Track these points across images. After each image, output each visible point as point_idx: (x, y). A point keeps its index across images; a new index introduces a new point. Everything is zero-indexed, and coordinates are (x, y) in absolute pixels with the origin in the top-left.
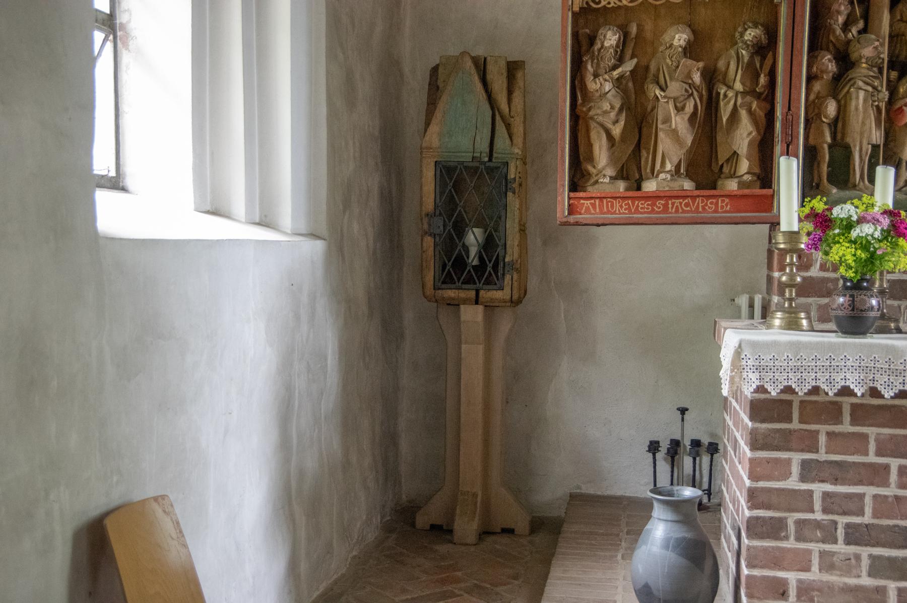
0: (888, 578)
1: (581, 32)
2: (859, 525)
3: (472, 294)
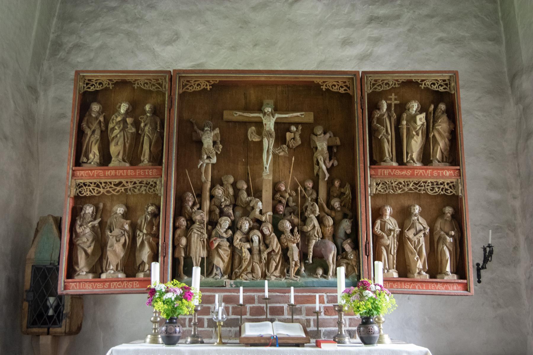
3: (46, 330)
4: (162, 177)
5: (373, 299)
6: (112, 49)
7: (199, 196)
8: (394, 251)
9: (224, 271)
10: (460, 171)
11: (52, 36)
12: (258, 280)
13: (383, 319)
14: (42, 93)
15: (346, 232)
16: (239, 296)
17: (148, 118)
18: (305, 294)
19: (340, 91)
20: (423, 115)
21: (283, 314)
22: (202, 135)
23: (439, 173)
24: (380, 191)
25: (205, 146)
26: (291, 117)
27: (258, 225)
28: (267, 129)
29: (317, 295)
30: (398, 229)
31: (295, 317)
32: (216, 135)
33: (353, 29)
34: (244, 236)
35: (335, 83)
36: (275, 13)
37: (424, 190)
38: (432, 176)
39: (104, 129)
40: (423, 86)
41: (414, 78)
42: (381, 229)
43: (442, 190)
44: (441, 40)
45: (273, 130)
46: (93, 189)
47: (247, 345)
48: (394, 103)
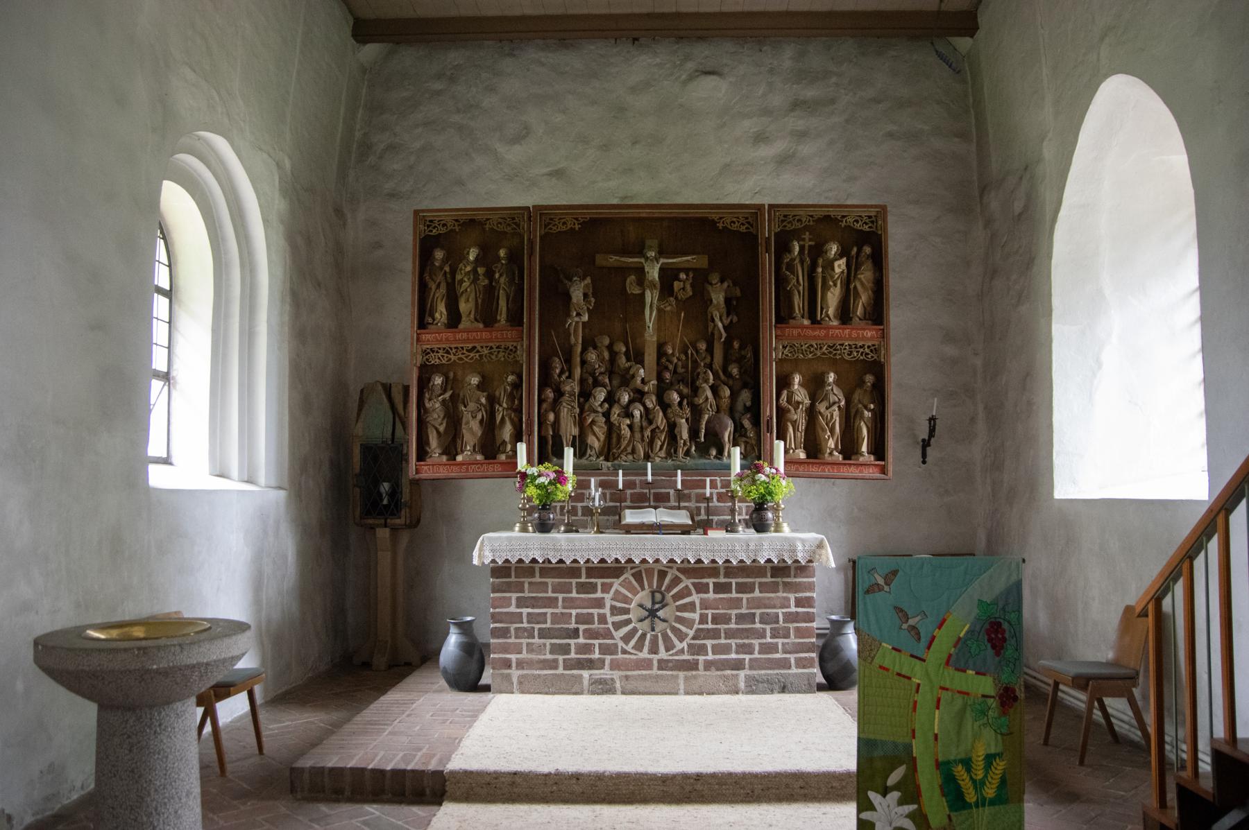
0: (559, 654)
1: (424, 376)
2: (545, 628)
3: (383, 521)
4: (523, 340)
5: (766, 484)
6: (438, 150)
7: (568, 360)
8: (802, 427)
9: (599, 451)
10: (884, 332)
11: (358, 135)
12: (640, 462)
13: (783, 506)
14: (349, 216)
15: (745, 405)
16: (618, 481)
17: (504, 267)
18: (695, 478)
19: (741, 230)
20: (844, 260)
21: (669, 501)
22: (570, 286)
23: (858, 334)
24: (787, 355)
25: (574, 300)
26: (680, 263)
27: (639, 396)
28: (650, 279)
29: (708, 480)
30: (807, 401)
31: (682, 504)
32: (587, 286)
33: (770, 119)
34: (623, 410)
35: (735, 219)
36: (662, 96)
37: (840, 355)
38: (850, 338)
39: (450, 281)
40: (843, 224)
41: (833, 213)
42: (788, 402)
43: (862, 355)
44: (890, 135)
45: (657, 279)
46: (443, 356)
47: (628, 532)
48: (808, 244)
